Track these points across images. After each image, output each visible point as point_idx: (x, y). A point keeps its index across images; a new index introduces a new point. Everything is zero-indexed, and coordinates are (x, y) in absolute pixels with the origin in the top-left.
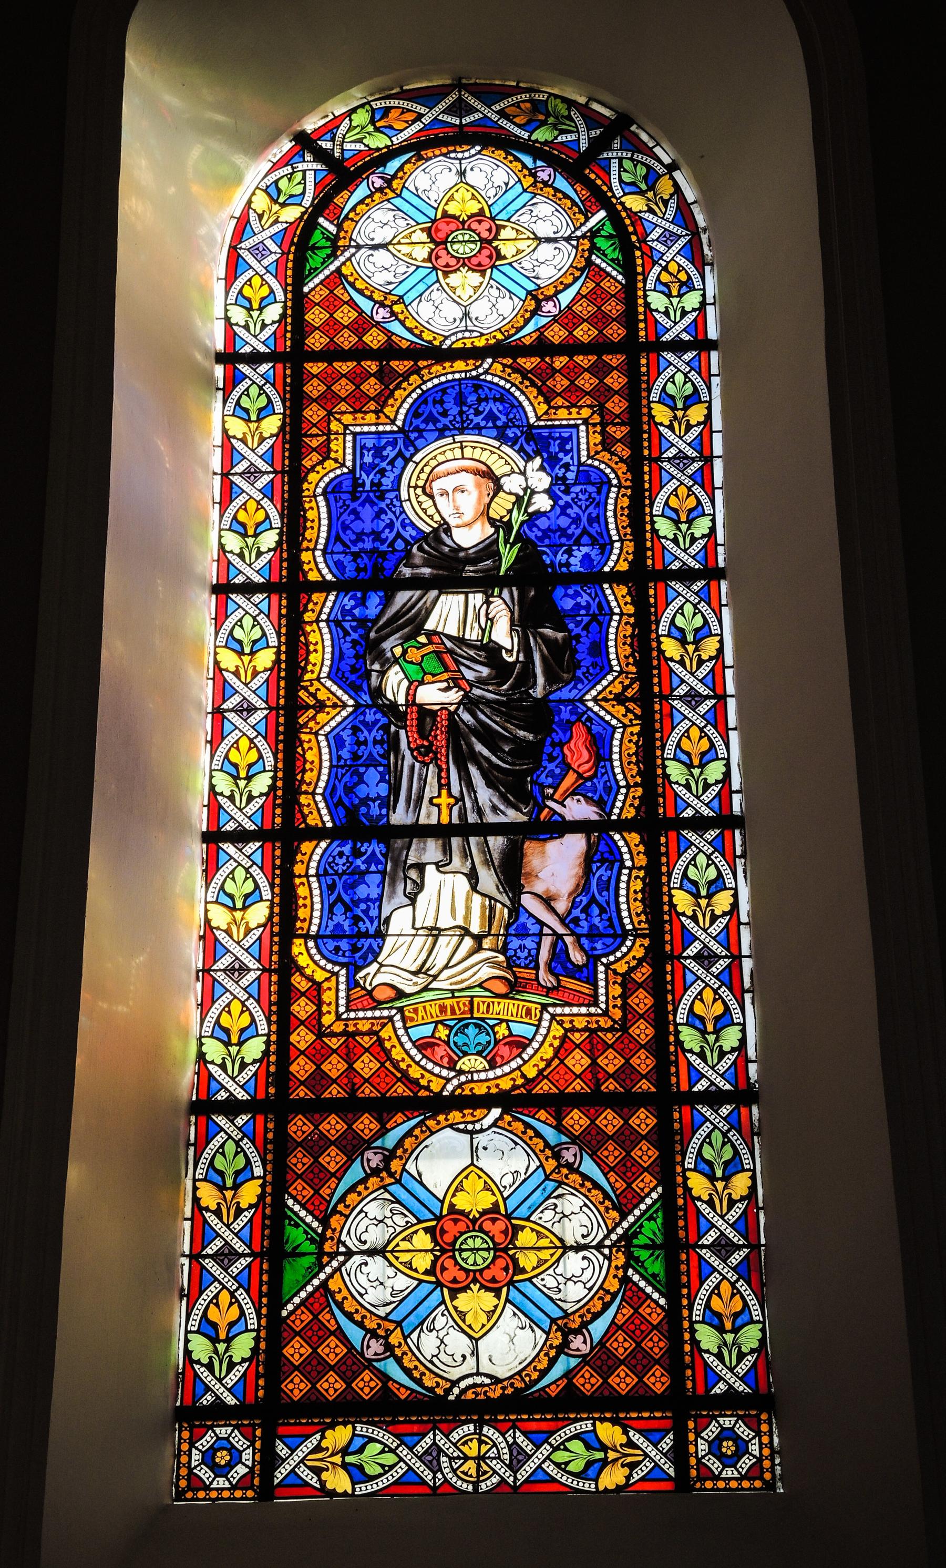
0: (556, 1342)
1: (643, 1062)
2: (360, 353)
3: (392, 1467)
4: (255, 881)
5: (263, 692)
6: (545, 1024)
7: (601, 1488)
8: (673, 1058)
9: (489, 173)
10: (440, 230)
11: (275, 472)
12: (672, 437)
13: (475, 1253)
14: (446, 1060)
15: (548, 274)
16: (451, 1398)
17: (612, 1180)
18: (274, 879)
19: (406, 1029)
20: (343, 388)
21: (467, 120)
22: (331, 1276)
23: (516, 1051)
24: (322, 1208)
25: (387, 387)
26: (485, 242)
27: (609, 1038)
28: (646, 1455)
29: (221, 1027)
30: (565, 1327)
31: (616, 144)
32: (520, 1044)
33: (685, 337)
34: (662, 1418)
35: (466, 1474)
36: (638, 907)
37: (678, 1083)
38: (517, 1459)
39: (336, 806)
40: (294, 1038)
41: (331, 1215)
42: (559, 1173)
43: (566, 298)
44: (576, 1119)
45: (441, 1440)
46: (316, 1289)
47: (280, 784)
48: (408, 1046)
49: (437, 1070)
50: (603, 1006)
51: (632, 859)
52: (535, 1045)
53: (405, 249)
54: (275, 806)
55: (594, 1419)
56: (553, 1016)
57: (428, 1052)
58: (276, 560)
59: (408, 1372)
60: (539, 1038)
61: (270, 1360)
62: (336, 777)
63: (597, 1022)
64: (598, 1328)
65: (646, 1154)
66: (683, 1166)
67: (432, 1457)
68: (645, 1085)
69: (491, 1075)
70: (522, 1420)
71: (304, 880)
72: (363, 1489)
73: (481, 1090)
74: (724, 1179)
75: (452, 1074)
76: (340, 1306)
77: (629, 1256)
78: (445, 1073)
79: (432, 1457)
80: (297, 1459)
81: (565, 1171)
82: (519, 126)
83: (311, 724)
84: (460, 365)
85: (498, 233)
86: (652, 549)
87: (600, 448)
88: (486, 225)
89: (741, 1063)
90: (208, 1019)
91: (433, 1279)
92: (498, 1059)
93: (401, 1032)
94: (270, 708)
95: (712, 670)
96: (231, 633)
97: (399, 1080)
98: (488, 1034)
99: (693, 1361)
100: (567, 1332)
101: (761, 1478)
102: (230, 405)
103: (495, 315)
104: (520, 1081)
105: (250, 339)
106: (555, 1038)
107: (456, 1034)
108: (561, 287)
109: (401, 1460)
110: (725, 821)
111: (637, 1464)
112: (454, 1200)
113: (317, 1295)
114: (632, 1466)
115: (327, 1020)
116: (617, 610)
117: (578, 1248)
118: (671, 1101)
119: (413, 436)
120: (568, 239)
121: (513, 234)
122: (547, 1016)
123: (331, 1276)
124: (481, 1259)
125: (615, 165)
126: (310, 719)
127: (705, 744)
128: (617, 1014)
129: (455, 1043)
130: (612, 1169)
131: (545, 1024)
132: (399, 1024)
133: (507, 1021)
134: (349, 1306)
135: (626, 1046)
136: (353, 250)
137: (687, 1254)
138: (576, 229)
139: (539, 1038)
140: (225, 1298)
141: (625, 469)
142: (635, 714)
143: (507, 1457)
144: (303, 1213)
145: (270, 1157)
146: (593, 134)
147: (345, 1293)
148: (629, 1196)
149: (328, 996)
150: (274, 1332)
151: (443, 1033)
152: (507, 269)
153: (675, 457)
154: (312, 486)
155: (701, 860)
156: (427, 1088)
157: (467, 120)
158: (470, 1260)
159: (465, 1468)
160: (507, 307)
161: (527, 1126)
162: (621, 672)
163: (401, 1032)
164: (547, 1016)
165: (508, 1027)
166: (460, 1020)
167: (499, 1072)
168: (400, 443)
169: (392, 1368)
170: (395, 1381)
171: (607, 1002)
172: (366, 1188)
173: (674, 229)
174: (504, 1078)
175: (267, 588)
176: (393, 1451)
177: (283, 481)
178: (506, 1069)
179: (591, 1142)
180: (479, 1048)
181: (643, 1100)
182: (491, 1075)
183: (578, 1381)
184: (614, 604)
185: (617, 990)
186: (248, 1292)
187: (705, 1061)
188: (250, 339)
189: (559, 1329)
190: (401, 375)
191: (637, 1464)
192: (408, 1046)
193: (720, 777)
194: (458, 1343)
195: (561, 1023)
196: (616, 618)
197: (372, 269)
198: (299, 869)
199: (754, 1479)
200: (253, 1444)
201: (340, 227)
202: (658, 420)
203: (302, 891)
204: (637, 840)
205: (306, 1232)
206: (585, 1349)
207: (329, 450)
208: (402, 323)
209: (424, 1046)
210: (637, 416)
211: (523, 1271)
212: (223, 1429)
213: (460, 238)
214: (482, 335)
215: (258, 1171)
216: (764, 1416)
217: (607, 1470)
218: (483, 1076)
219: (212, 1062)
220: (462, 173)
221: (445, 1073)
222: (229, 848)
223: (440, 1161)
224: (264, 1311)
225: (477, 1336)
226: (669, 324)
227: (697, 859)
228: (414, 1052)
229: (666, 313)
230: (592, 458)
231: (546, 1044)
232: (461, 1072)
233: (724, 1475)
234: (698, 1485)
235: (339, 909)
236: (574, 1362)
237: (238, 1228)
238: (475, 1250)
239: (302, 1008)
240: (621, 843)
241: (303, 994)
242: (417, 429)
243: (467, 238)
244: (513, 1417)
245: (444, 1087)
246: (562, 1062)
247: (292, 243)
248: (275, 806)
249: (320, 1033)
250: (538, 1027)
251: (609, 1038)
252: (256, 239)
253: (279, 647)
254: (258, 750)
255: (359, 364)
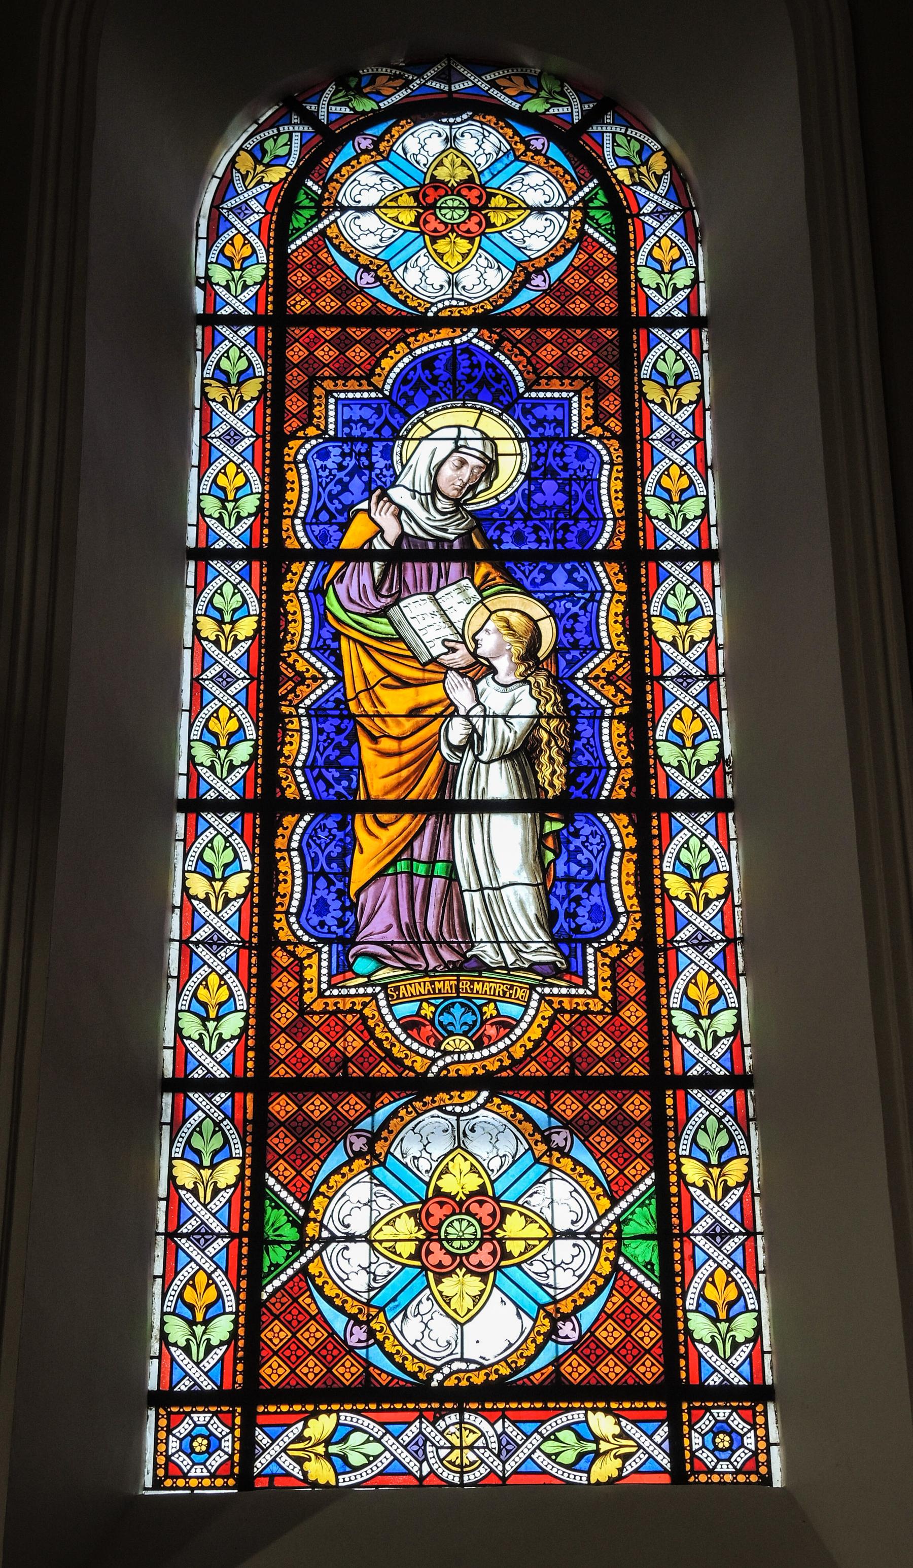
0: (543, 1330)
1: (636, 1044)
2: (343, 319)
3: (376, 1457)
4: (248, 359)
5: (250, 420)
6: (534, 1004)
7: (593, 1481)
8: (666, 1042)
9: (479, 143)
10: (427, 195)
11: (232, 1236)
12: (690, 915)
13: (452, 211)
14: (432, 1040)
15: (537, 246)
16: (430, 314)
17: (604, 1166)
18: (249, 988)
19: (390, 1006)
20: (325, 353)
21: (456, 87)
22: (311, 1261)
23: (503, 1032)
24: (305, 1190)
25: (373, 354)
26: (473, 209)
27: (600, 1020)
28: (640, 1447)
29: (185, 1303)
30: (554, 1314)
31: (608, 118)
32: (507, 1025)
33: (677, 313)
34: (656, 1409)
35: (453, 1464)
36: (630, 890)
37: (672, 1067)
38: (506, 1448)
39: (316, 780)
40: (266, 1335)
41: (314, 1197)
42: (546, 1152)
43: (556, 271)
44: (569, 1105)
45: (428, 1429)
46: (296, 1273)
47: (241, 1332)
48: (393, 1025)
49: (422, 1050)
50: (593, 988)
51: (622, 841)
52: (523, 1025)
53: (392, 213)
54: (247, 1049)
55: (586, 1409)
56: (542, 996)
57: (414, 1033)
58: (251, 774)
59: (390, 1356)
60: (528, 1019)
61: (249, 1346)
62: (318, 749)
63: (587, 1005)
64: (588, 1315)
65: (638, 1141)
66: (677, 1153)
67: (419, 1447)
68: (636, 1069)
69: (477, 1055)
70: (510, 1409)
71: (285, 854)
72: (346, 1480)
73: (467, 1071)
74: (719, 1163)
75: (438, 1054)
76: (320, 1290)
77: (586, 215)
78: (430, 1053)
79: (419, 1447)
80: (278, 1449)
81: (556, 1155)
82: (510, 97)
83: (290, 697)
84: (445, 332)
85: (488, 201)
86: (636, 297)
87: (591, 422)
88: (476, 193)
89: (704, 528)
90: (171, 1292)
91: (418, 1263)
92: (485, 1040)
93: (385, 1011)
94: (252, 679)
95: (698, 528)
96: (214, 481)
97: (383, 1059)
98: (474, 1013)
99: (687, 1352)
100: (557, 1319)
101: (757, 1472)
102: (199, 724)
103: (482, 286)
104: (507, 1062)
105: (231, 300)
106: (543, 1018)
107: (441, 1014)
108: (551, 260)
109: (386, 1449)
110: (693, 321)
111: (630, 1455)
112: (440, 1183)
113: (296, 1279)
114: (626, 1457)
115: (308, 998)
116: (608, 588)
117: (570, 1234)
118: (663, 1081)
119: (402, 403)
120: (559, 210)
121: (503, 203)
122: (536, 996)
123: (311, 1261)
124: (459, 216)
125: (608, 138)
126: (290, 692)
127: (685, 482)
128: (607, 996)
129: (441, 1023)
130: (604, 1155)
131: (534, 1004)
132: (383, 1003)
133: (495, 1001)
134: (329, 1291)
135: (619, 1031)
136: (337, 214)
137: (682, 1242)
138: (569, 198)
139: (528, 1019)
140: (214, 980)
141: (617, 446)
142: (625, 694)
143: (496, 1445)
144: (284, 1194)
145: (249, 1139)
146: (586, 107)
147: (325, 1277)
148: (621, 1183)
149: (309, 974)
150: (253, 1315)
151: (427, 1010)
152: (496, 238)
153: (678, 676)
154: (292, 452)
155: (681, 590)
156: (412, 1069)
157: (456, 87)
158: (447, 215)
159: (452, 1457)
160: (495, 279)
161: (517, 1109)
162: (613, 651)
163: (385, 1011)
164: (536, 996)
165: (496, 1008)
166: (446, 999)
167: (485, 1052)
168: (386, 411)
169: (375, 1355)
170: (376, 1367)
171: (596, 984)
172: (351, 1170)
173: (667, 204)
174: (491, 1057)
175: (248, 554)
176: (378, 1441)
177: (258, 689)
178: (494, 1050)
179: (582, 1127)
180: (466, 1028)
181: (635, 1084)
182: (477, 1055)
183: (565, 1369)
184: (605, 581)
185: (606, 973)
186: (236, 975)
187: (677, 649)
188: (231, 300)
189: (548, 1315)
190: (387, 342)
191: (630, 1455)
192: (393, 1025)
193: (699, 513)
194: (443, 1329)
195: (550, 1003)
196: (608, 595)
197: (358, 232)
198: (280, 843)
199: (750, 1473)
200: (232, 1431)
201: (324, 188)
202: (672, 893)
203: (283, 866)
204: (616, 570)
205: (287, 1214)
206: (575, 1336)
207: (311, 416)
208: (387, 288)
209: (410, 1025)
210: (630, 391)
211: (494, 225)
212: (202, 1416)
213: (450, 203)
214: (470, 304)
215: (247, 865)
216: (760, 1408)
217: (598, 1463)
218: (469, 1056)
219: (189, 1038)
220: (453, 283)
221: (430, 1053)
222: (219, 565)
223: (424, 1141)
224: (270, 361)
225: (462, 1321)
226: (661, 301)
227: (689, 843)
228: (398, 1031)
229: (658, 290)
230: (583, 432)
231: (535, 1025)
232: (446, 1053)
233: (718, 1469)
234: (692, 1479)
235: (322, 883)
236: (562, 1349)
237: (208, 1367)
238: (460, 1236)
239: (283, 984)
240: (610, 825)
241: (285, 969)
242: (405, 396)
243: (456, 204)
244: (501, 1406)
245: (429, 1068)
246: (550, 1044)
247: (276, 204)
248: (247, 1049)
249: (303, 1010)
250: (527, 1007)
251: (600, 1020)
252: (238, 200)
253: (263, 494)
254: (229, 988)
255: (344, 330)
